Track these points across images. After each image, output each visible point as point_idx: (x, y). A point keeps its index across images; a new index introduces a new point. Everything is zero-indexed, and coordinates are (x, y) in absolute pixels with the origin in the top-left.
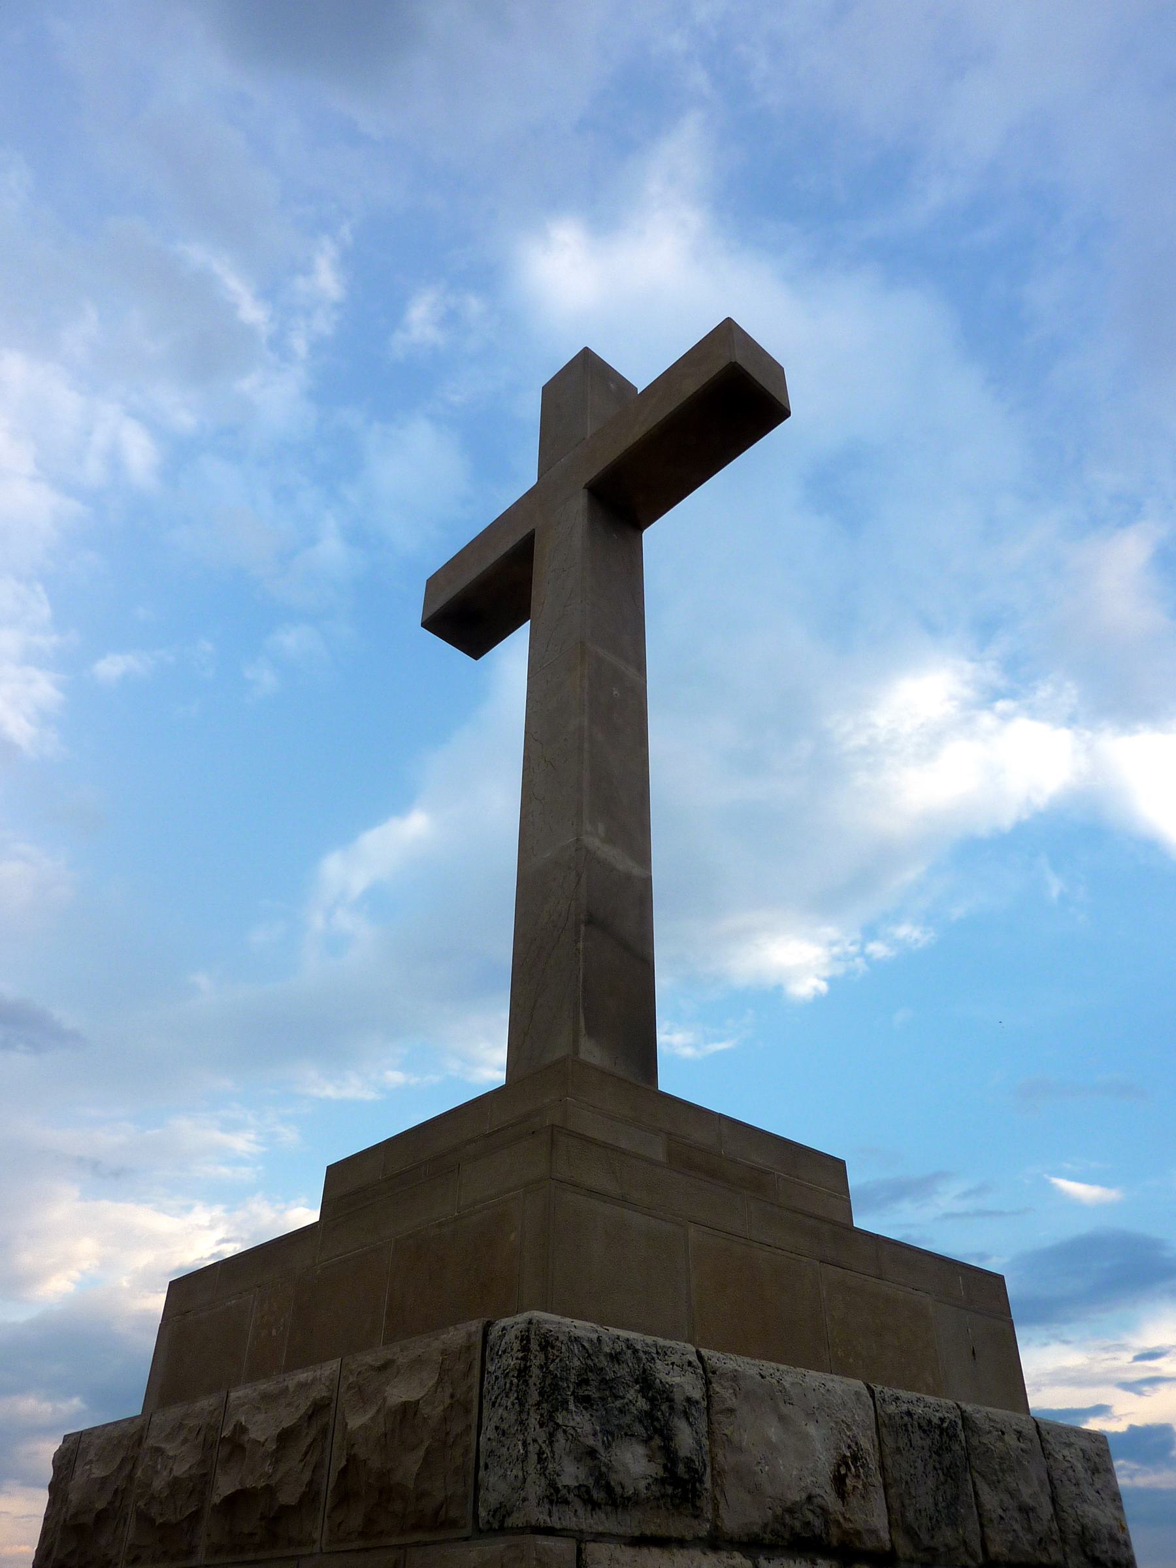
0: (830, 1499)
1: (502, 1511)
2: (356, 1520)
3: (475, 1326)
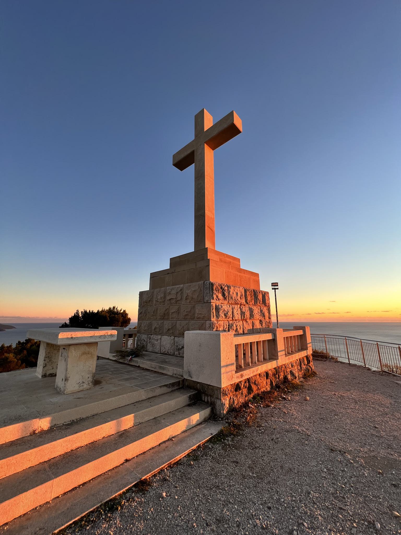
0: (240, 300)
1: (207, 301)
2: (188, 301)
3: (203, 282)
